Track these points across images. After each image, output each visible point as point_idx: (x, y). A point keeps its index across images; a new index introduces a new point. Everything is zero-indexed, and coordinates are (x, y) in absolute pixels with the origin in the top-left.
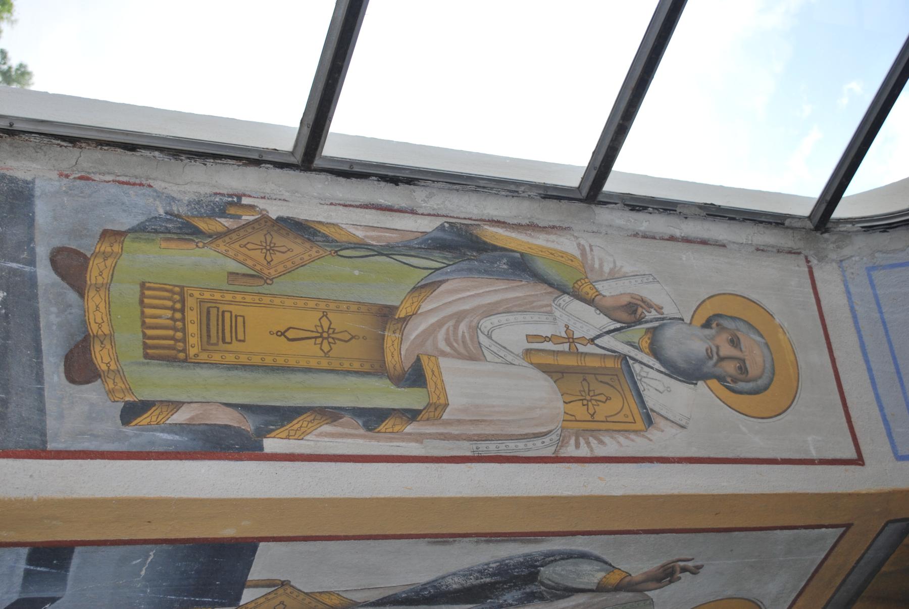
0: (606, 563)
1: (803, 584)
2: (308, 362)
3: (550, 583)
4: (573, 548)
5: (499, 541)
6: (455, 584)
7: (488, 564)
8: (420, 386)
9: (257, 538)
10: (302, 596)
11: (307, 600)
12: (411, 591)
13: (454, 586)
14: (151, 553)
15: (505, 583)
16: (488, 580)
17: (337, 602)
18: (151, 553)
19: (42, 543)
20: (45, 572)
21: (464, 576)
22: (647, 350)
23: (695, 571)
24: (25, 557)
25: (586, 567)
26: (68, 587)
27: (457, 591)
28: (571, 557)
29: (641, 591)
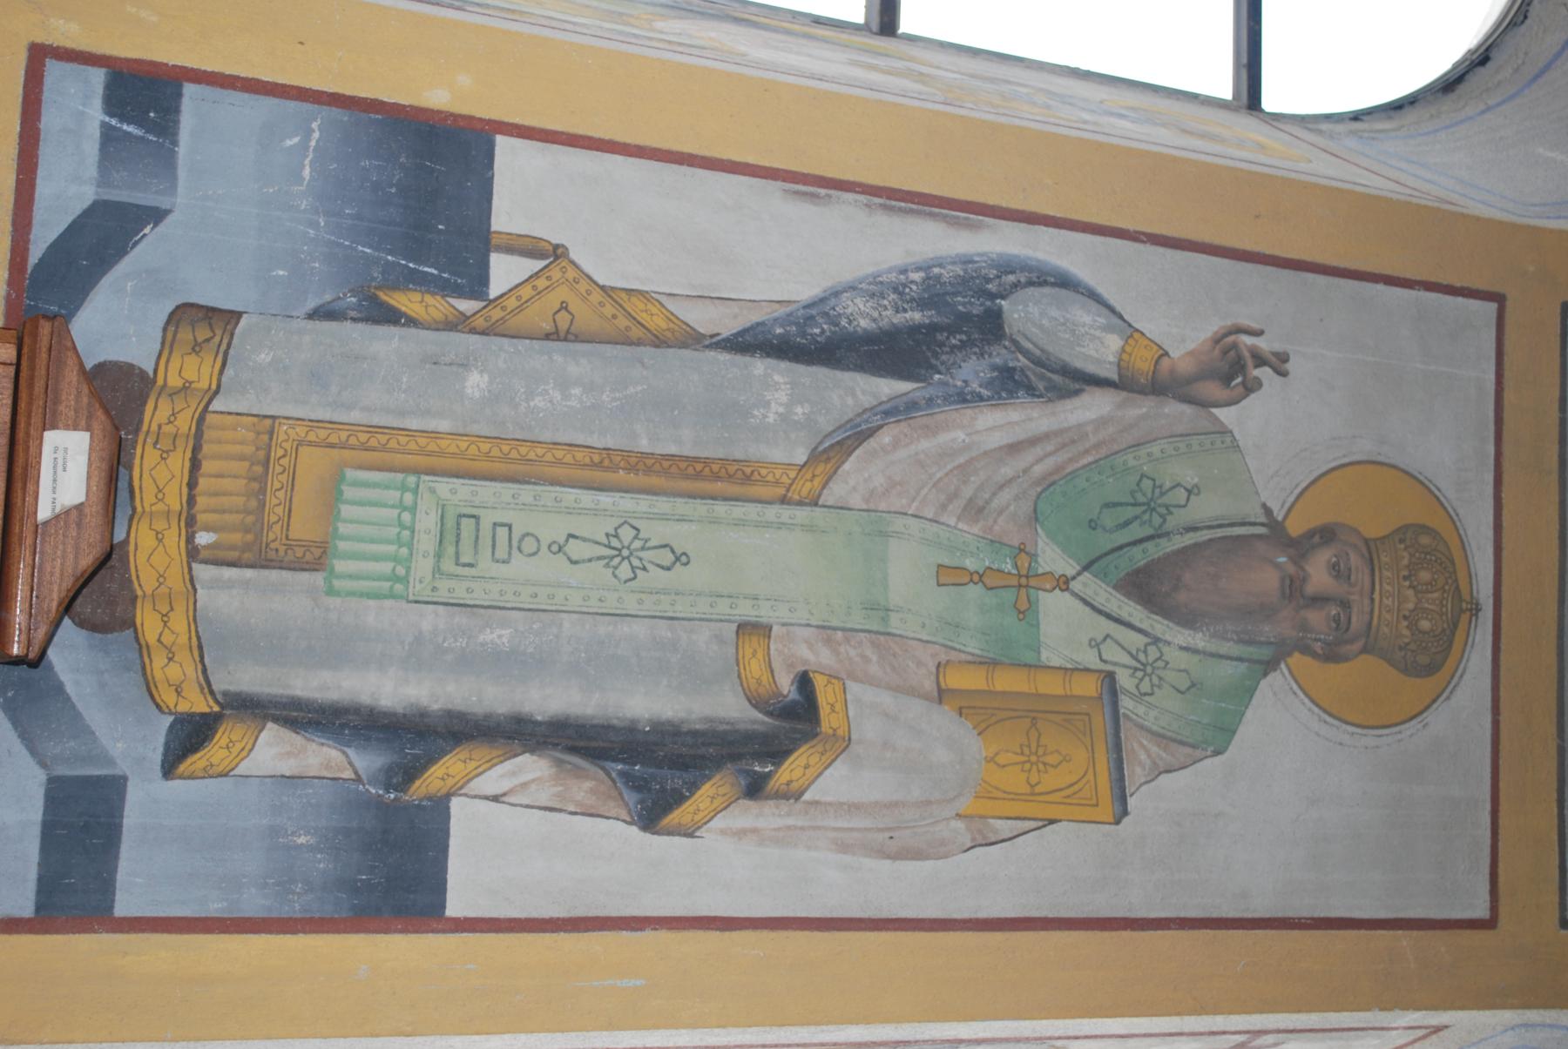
0: (1112, 310)
1: (1491, 449)
2: (549, 278)
3: (1038, 352)
4: (1040, 255)
5: (911, 211)
6: (862, 315)
7: (904, 271)
8: (125, 786)
9: (489, 122)
10: (597, 296)
11: (609, 310)
12: (787, 320)
13: (864, 323)
14: (314, 125)
15: (952, 330)
16: (916, 316)
17: (663, 325)
18: (314, 125)
19: (128, 60)
20: (136, 137)
21: (873, 295)
22: (71, 362)
23: (1279, 363)
24: (99, 90)
25: (1084, 316)
26: (180, 189)
27: (869, 338)
28: (1043, 283)
29: (1205, 404)
